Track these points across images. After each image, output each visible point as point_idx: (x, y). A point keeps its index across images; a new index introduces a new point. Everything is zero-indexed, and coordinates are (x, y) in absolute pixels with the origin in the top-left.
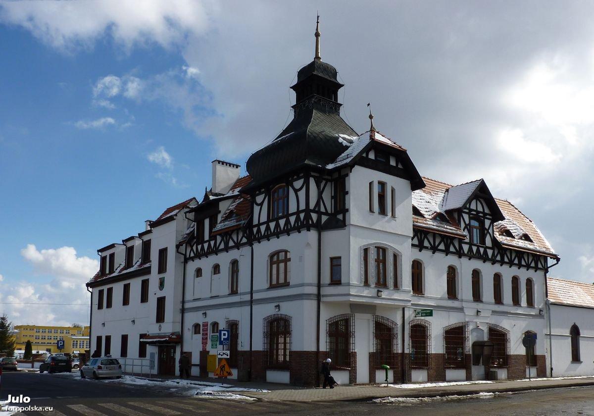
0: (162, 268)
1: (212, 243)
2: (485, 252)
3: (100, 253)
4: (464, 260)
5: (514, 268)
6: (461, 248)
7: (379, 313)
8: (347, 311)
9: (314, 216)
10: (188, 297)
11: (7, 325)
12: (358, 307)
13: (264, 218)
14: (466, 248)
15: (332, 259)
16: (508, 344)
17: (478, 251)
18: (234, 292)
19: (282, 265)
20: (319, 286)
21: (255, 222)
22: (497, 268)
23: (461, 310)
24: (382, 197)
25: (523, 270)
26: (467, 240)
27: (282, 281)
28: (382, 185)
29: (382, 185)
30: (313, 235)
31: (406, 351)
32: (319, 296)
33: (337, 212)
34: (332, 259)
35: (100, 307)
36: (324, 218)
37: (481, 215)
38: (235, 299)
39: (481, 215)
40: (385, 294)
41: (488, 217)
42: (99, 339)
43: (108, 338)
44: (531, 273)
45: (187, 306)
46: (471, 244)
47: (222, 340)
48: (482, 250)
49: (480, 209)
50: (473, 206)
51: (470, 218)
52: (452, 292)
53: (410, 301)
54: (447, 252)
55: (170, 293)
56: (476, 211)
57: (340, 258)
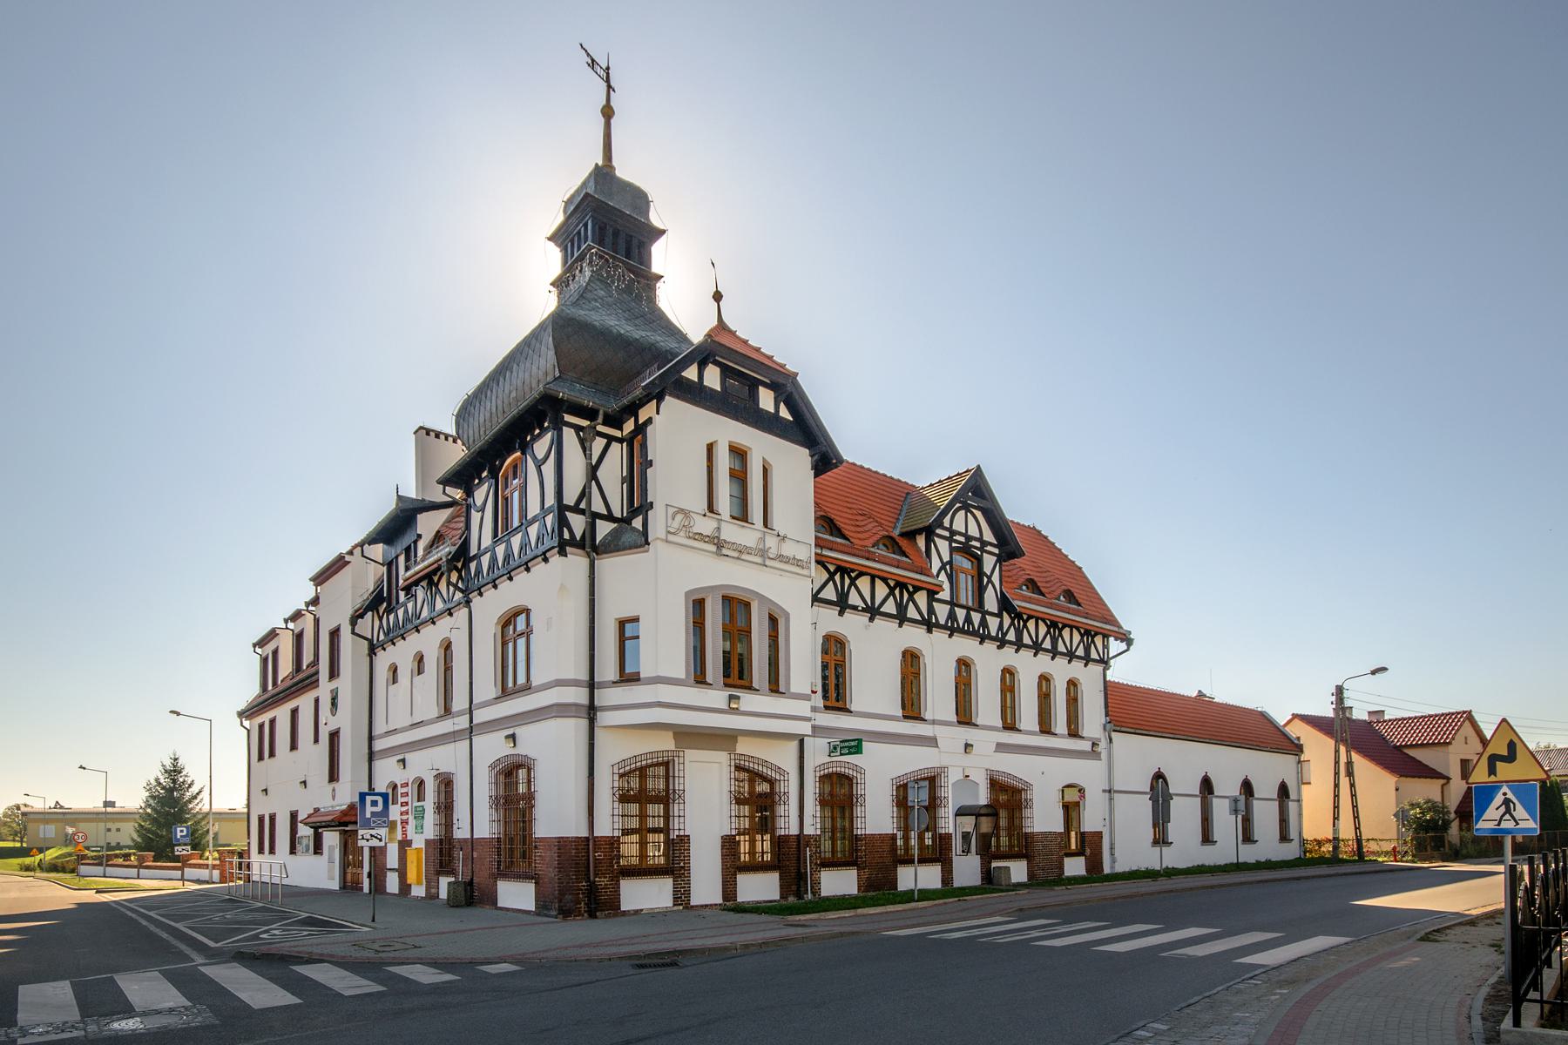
0: (334, 674)
1: (410, 606)
2: (984, 623)
3: (259, 650)
4: (939, 636)
5: (1044, 658)
6: (931, 611)
7: (744, 747)
8: (666, 743)
9: (578, 523)
10: (379, 728)
11: (188, 795)
12: (689, 736)
13: (487, 541)
14: (942, 612)
15: (622, 624)
16: (1027, 813)
17: (968, 620)
18: (447, 711)
19: (521, 642)
20: (592, 685)
21: (473, 551)
22: (1009, 656)
23: (932, 742)
24: (739, 477)
25: (1061, 661)
26: (945, 595)
27: (521, 680)
28: (739, 453)
29: (739, 453)
30: (576, 562)
31: (809, 830)
32: (591, 711)
33: (634, 512)
34: (622, 624)
35: (261, 758)
36: (604, 529)
37: (974, 543)
38: (446, 726)
39: (974, 543)
40: (748, 701)
41: (989, 548)
42: (261, 819)
43: (273, 818)
44: (1077, 669)
45: (379, 745)
46: (953, 603)
47: (368, 815)
48: (976, 617)
49: (973, 531)
50: (959, 525)
51: (952, 550)
52: (911, 707)
53: (809, 719)
54: (901, 617)
55: (346, 720)
56: (965, 535)
57: (636, 620)
